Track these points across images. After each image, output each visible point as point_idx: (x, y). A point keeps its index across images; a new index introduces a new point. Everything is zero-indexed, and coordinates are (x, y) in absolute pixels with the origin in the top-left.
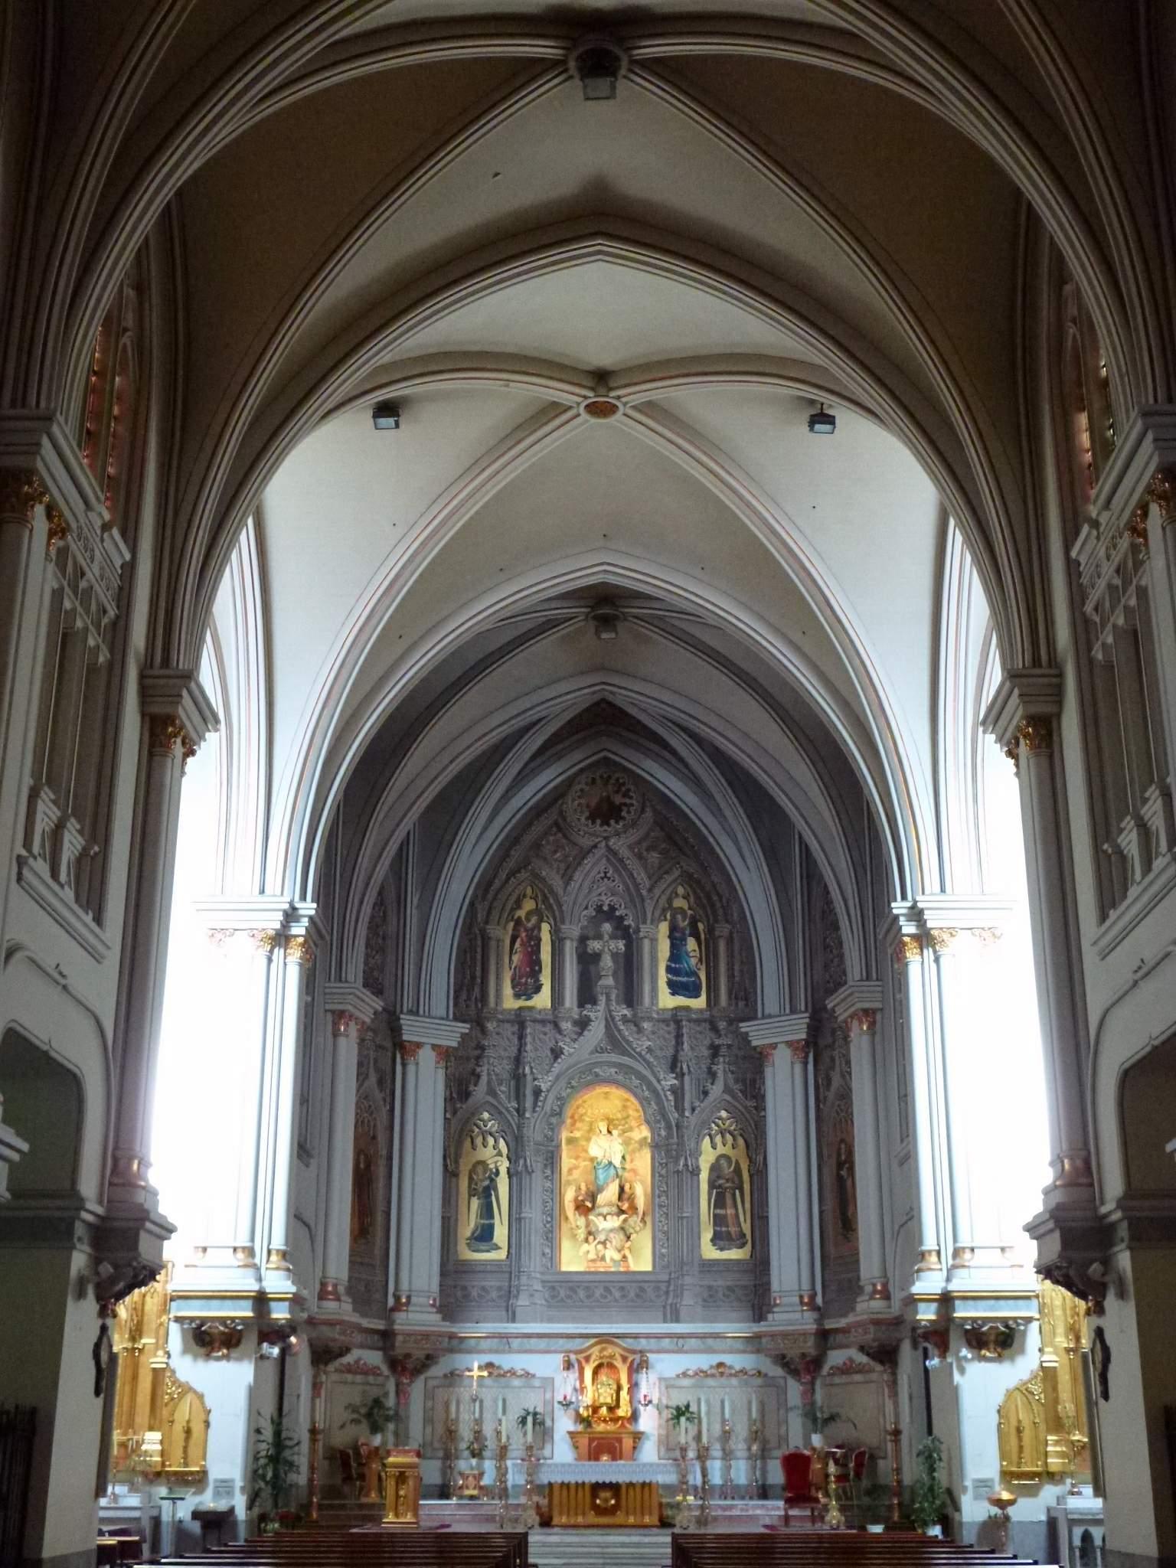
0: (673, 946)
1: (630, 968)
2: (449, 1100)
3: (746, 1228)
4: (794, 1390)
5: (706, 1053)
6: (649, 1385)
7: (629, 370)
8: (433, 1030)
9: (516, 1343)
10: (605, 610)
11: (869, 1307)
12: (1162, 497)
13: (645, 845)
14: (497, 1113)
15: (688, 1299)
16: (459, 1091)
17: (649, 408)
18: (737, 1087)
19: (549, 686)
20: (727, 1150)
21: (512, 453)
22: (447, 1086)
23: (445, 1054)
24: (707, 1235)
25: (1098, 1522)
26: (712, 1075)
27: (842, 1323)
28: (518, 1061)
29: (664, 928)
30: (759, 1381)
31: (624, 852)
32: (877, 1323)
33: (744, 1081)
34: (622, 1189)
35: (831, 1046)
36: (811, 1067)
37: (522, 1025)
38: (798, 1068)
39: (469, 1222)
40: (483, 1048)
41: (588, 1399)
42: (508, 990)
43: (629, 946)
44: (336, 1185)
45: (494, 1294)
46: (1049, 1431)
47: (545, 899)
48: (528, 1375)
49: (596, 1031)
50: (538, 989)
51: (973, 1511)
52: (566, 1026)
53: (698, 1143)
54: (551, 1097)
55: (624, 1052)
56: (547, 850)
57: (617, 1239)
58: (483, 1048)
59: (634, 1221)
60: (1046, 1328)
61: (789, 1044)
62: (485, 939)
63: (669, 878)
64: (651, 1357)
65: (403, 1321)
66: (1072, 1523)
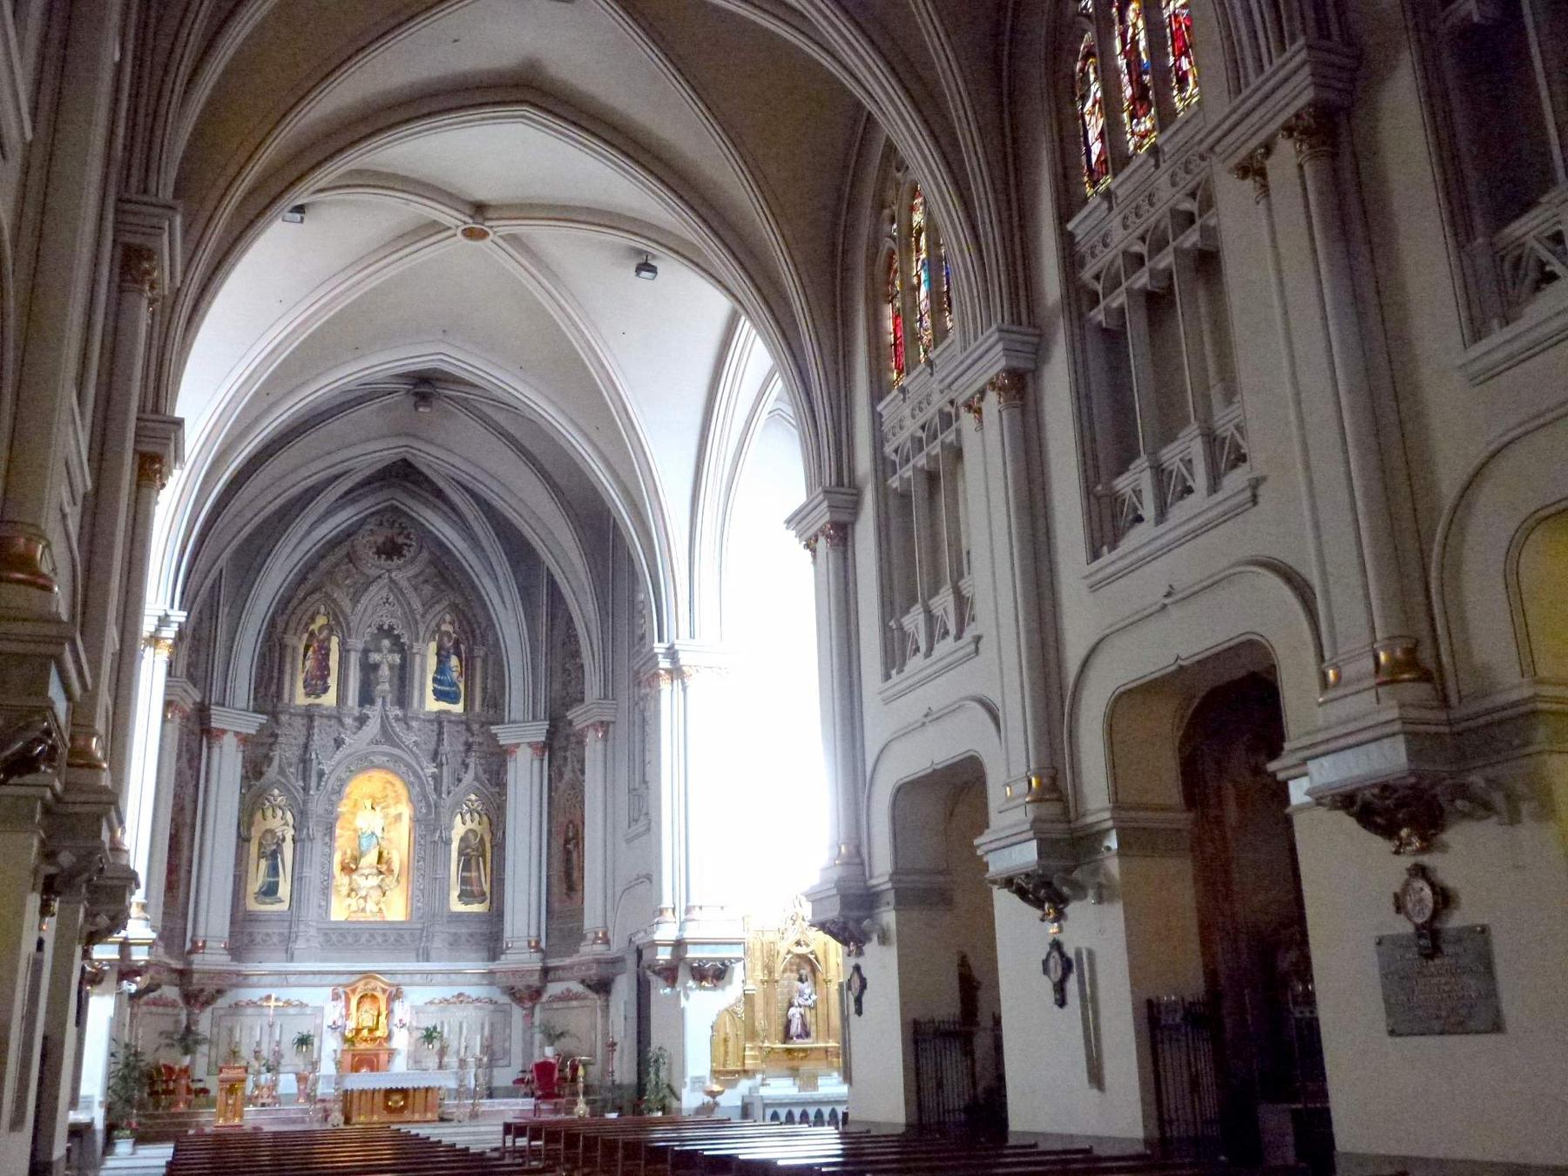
0: (440, 662)
1: (403, 677)
2: (245, 778)
3: (486, 888)
4: (517, 1013)
5: (462, 748)
6: (401, 1010)
7: (509, 206)
8: (236, 719)
9: (292, 979)
10: (424, 389)
11: (590, 950)
12: (1002, 390)
13: (421, 578)
14: (286, 790)
15: (437, 943)
16: (254, 770)
17: (513, 239)
18: (484, 777)
19: (365, 446)
20: (469, 825)
21: (395, 256)
22: (244, 766)
23: (244, 740)
24: (455, 893)
25: (845, 1102)
26: (466, 766)
27: (567, 961)
28: (306, 747)
29: (433, 646)
30: (492, 1007)
31: (404, 584)
32: (598, 962)
33: (491, 773)
34: (380, 855)
35: (565, 749)
36: (546, 763)
37: (311, 718)
38: (536, 764)
39: (258, 877)
40: (276, 736)
41: (352, 1024)
42: (300, 689)
43: (404, 659)
44: (599, 874)
45: (275, 939)
46: (746, 1039)
47: (336, 617)
48: (302, 1005)
49: (373, 727)
50: (326, 689)
51: (690, 1100)
52: (348, 721)
53: (452, 819)
54: (333, 778)
55: (394, 745)
56: (339, 577)
57: (376, 894)
58: (276, 736)
59: (390, 880)
60: (748, 965)
61: (530, 745)
62: (283, 647)
63: (438, 608)
64: (404, 988)
65: (198, 961)
66: (766, 1106)
